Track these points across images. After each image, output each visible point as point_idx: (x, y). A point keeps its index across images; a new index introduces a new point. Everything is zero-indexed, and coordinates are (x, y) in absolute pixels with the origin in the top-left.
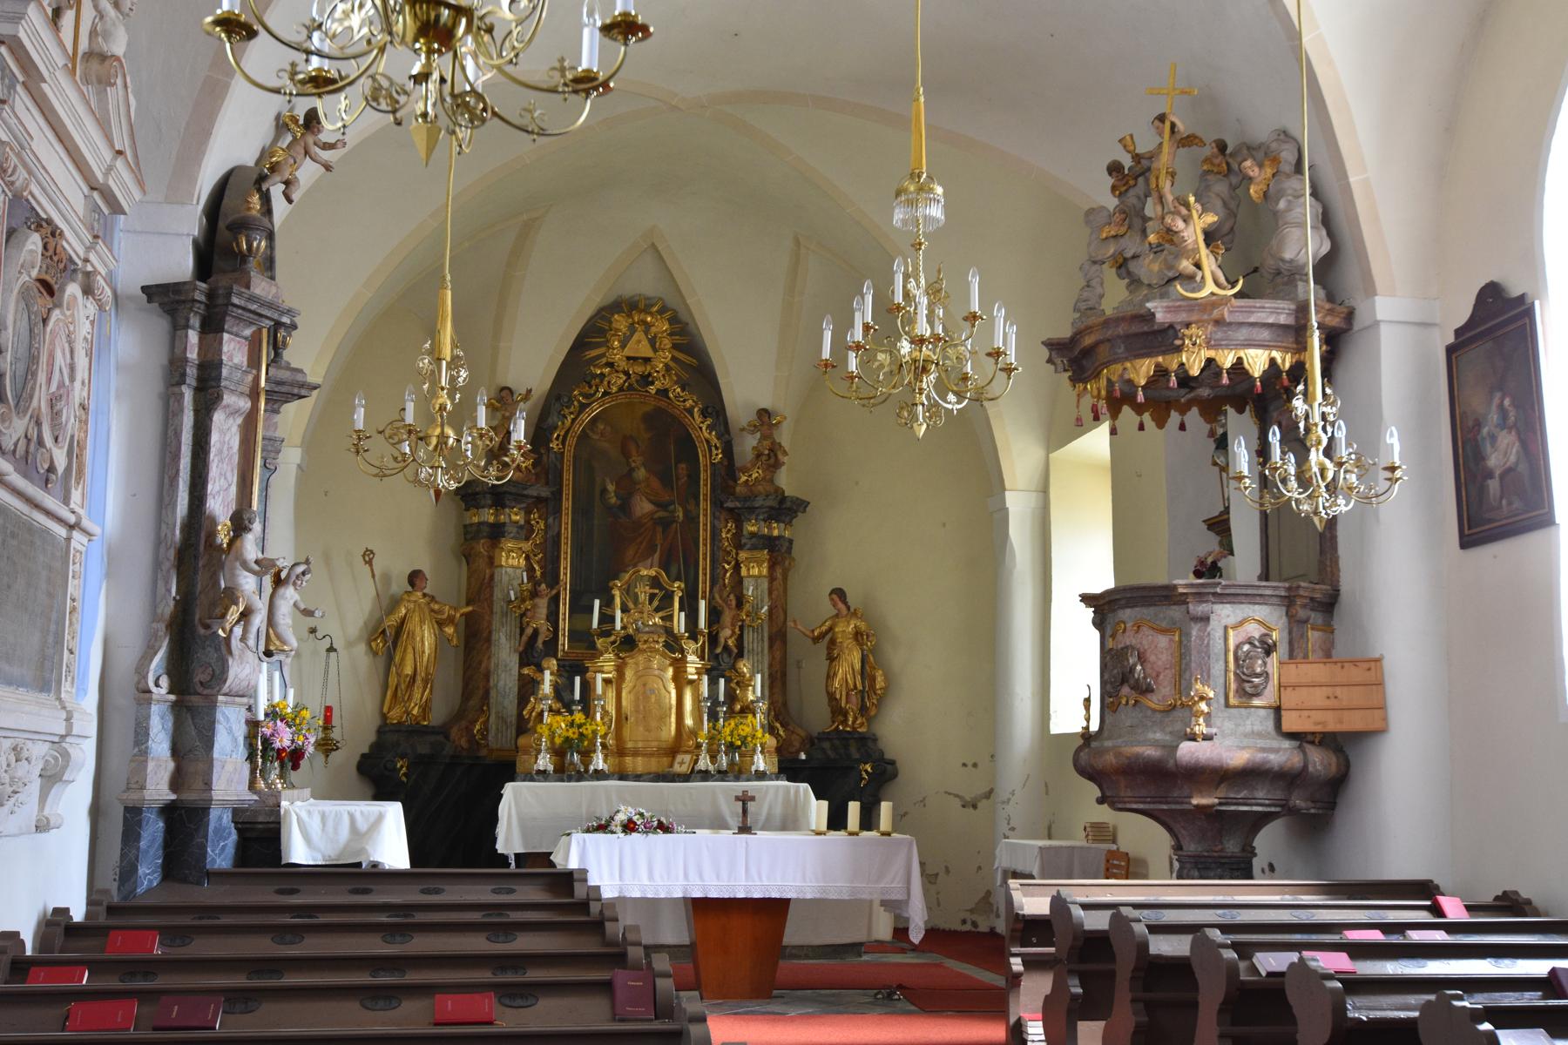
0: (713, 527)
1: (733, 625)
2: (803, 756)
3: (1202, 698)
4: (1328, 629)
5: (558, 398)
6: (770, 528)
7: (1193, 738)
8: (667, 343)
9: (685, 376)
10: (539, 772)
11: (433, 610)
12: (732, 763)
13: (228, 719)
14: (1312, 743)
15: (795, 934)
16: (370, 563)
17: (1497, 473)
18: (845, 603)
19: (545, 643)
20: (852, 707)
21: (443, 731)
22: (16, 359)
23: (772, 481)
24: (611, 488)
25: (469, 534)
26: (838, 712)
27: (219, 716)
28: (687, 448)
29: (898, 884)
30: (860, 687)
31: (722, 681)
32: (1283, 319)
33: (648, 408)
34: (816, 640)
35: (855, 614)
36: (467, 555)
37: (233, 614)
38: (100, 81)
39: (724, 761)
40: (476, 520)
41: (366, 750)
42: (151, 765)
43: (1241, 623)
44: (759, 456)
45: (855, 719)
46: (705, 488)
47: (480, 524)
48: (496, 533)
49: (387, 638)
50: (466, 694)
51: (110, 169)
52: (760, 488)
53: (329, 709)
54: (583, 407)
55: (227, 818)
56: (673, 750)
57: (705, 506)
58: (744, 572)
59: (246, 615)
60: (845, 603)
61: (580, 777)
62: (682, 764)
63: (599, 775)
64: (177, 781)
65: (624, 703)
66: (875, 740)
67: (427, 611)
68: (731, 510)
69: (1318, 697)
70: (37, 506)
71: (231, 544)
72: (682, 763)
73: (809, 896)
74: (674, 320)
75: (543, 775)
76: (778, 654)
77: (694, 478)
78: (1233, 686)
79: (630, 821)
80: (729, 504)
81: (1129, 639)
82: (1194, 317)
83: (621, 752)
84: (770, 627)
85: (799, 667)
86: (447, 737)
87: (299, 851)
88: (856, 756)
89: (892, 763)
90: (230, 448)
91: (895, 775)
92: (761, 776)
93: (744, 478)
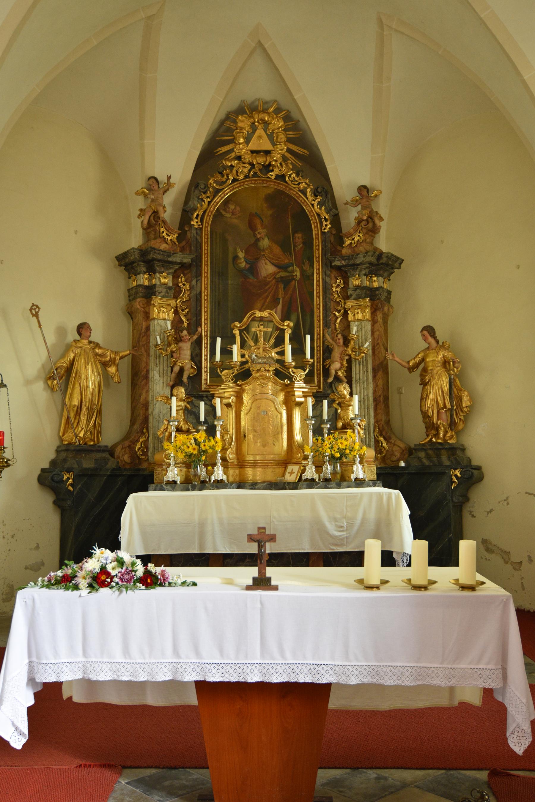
1: (341, 359)
2: (402, 464)
5: (197, 187)
6: (371, 281)
8: (282, 137)
9: (299, 164)
10: (168, 483)
11: (97, 354)
12: (334, 473)
16: (36, 315)
18: (434, 337)
19: (189, 378)
20: (443, 422)
21: (111, 451)
23: (372, 243)
24: (241, 255)
25: (132, 294)
26: (431, 427)
28: (302, 220)
29: (488, 664)
30: (448, 406)
31: (325, 402)
33: (269, 191)
34: (411, 369)
35: (443, 346)
36: (131, 313)
40: (135, 284)
41: (46, 466)
45: (446, 432)
46: (317, 253)
47: (138, 286)
48: (149, 292)
49: (61, 376)
50: (133, 422)
52: (361, 248)
54: (217, 191)
56: (285, 463)
57: (318, 265)
58: (351, 317)
60: (434, 337)
61: (203, 485)
62: (292, 474)
63: (219, 484)
65: (243, 423)
66: (463, 450)
67: (91, 355)
68: (339, 269)
72: (291, 473)
73: (354, 681)
74: (287, 118)
75: (172, 485)
76: (380, 383)
77: (308, 244)
79: (103, 570)
80: (337, 263)
83: (241, 464)
84: (374, 360)
85: (400, 393)
86: (112, 454)
88: (447, 463)
89: (479, 468)
91: (481, 479)
93: (348, 242)
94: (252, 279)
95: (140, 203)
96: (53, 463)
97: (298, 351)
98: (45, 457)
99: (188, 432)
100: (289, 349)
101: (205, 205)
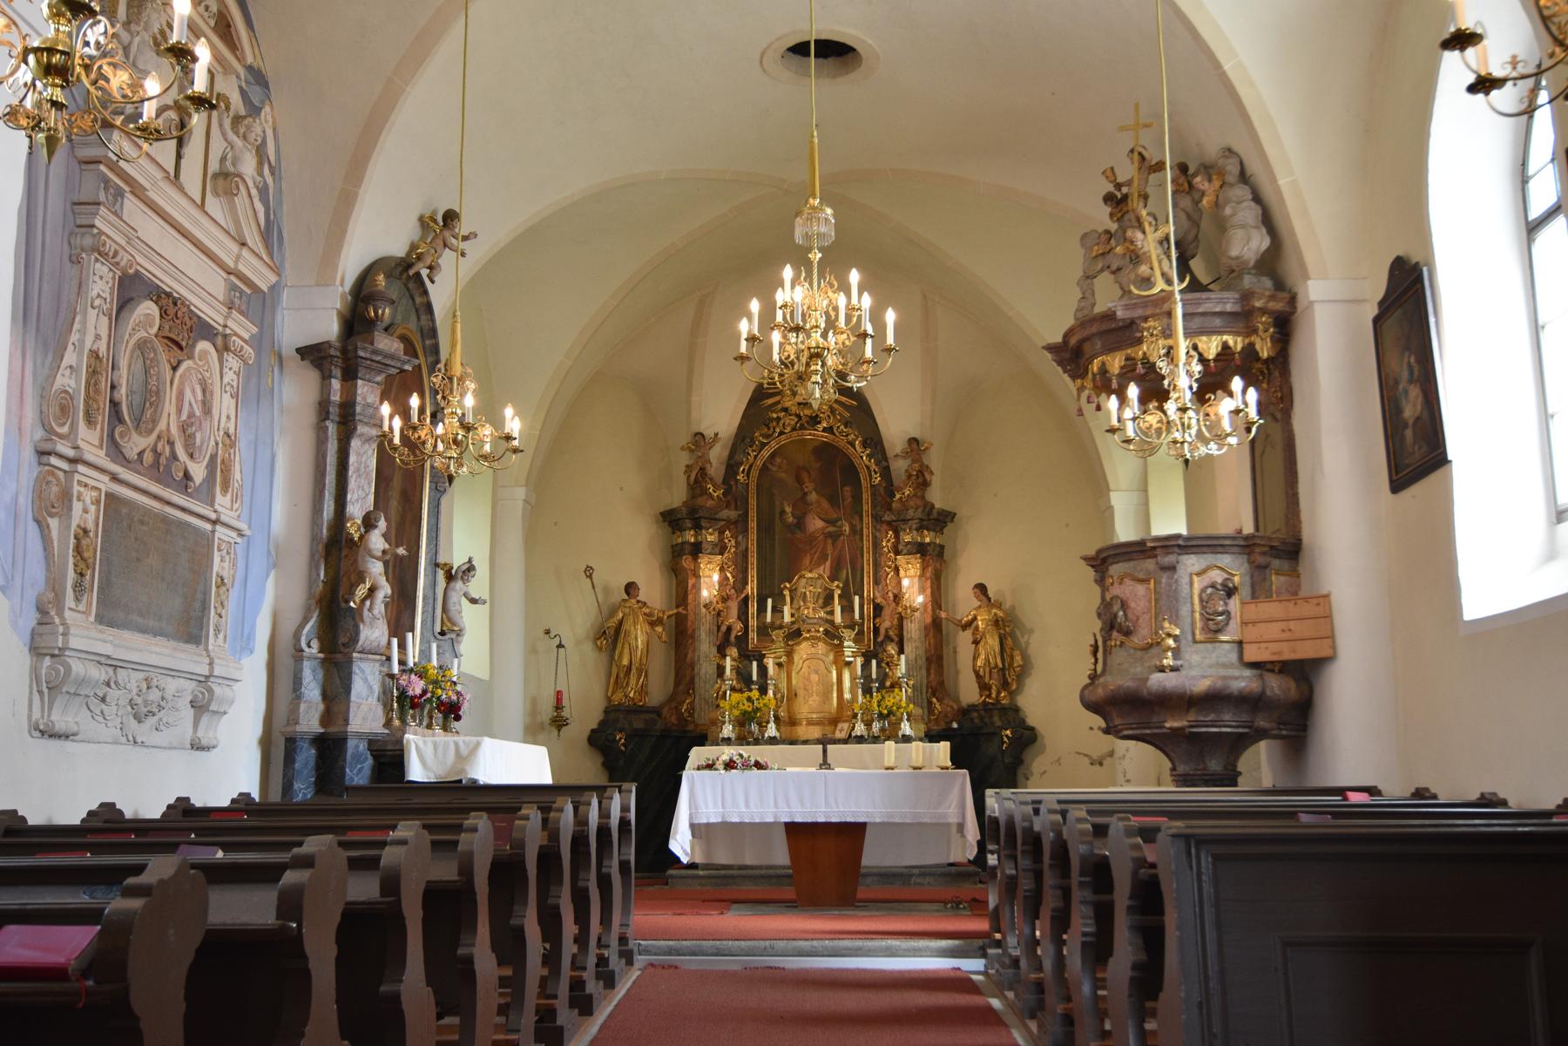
0: (875, 537)
2: (955, 725)
3: (1169, 635)
4: (1294, 573)
6: (923, 537)
7: (1162, 669)
12: (882, 730)
13: (363, 671)
14: (1272, 671)
15: (873, 857)
16: (590, 577)
17: (1411, 422)
21: (656, 711)
22: (130, 393)
23: (923, 497)
26: (984, 687)
27: (355, 669)
31: (874, 662)
32: (1229, 308)
37: (361, 591)
38: (225, 193)
39: (876, 727)
42: (303, 707)
43: (1204, 571)
44: (910, 476)
45: (999, 693)
46: (867, 507)
48: (697, 550)
49: (609, 636)
50: (677, 683)
51: (238, 257)
53: (559, 694)
54: (763, 445)
55: (363, 746)
56: (834, 722)
59: (372, 591)
61: (757, 742)
63: (773, 741)
64: (326, 718)
68: (889, 523)
69: (1274, 630)
70: (169, 503)
71: (362, 537)
77: (857, 498)
78: (1199, 625)
79: (731, 760)
80: (886, 518)
81: (1116, 590)
82: (1149, 312)
83: (793, 722)
86: (659, 715)
87: (416, 772)
88: (998, 723)
89: (1032, 729)
90: (367, 467)
92: (907, 739)
94: (799, 535)
95: (684, 459)
96: (602, 723)
97: (847, 609)
98: (593, 719)
99: (741, 691)
100: (838, 609)
101: (751, 459)
